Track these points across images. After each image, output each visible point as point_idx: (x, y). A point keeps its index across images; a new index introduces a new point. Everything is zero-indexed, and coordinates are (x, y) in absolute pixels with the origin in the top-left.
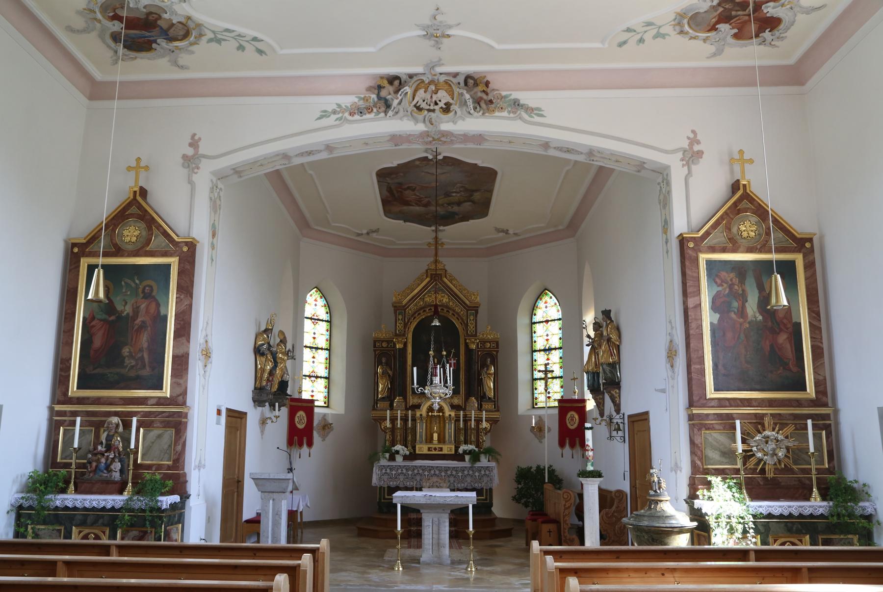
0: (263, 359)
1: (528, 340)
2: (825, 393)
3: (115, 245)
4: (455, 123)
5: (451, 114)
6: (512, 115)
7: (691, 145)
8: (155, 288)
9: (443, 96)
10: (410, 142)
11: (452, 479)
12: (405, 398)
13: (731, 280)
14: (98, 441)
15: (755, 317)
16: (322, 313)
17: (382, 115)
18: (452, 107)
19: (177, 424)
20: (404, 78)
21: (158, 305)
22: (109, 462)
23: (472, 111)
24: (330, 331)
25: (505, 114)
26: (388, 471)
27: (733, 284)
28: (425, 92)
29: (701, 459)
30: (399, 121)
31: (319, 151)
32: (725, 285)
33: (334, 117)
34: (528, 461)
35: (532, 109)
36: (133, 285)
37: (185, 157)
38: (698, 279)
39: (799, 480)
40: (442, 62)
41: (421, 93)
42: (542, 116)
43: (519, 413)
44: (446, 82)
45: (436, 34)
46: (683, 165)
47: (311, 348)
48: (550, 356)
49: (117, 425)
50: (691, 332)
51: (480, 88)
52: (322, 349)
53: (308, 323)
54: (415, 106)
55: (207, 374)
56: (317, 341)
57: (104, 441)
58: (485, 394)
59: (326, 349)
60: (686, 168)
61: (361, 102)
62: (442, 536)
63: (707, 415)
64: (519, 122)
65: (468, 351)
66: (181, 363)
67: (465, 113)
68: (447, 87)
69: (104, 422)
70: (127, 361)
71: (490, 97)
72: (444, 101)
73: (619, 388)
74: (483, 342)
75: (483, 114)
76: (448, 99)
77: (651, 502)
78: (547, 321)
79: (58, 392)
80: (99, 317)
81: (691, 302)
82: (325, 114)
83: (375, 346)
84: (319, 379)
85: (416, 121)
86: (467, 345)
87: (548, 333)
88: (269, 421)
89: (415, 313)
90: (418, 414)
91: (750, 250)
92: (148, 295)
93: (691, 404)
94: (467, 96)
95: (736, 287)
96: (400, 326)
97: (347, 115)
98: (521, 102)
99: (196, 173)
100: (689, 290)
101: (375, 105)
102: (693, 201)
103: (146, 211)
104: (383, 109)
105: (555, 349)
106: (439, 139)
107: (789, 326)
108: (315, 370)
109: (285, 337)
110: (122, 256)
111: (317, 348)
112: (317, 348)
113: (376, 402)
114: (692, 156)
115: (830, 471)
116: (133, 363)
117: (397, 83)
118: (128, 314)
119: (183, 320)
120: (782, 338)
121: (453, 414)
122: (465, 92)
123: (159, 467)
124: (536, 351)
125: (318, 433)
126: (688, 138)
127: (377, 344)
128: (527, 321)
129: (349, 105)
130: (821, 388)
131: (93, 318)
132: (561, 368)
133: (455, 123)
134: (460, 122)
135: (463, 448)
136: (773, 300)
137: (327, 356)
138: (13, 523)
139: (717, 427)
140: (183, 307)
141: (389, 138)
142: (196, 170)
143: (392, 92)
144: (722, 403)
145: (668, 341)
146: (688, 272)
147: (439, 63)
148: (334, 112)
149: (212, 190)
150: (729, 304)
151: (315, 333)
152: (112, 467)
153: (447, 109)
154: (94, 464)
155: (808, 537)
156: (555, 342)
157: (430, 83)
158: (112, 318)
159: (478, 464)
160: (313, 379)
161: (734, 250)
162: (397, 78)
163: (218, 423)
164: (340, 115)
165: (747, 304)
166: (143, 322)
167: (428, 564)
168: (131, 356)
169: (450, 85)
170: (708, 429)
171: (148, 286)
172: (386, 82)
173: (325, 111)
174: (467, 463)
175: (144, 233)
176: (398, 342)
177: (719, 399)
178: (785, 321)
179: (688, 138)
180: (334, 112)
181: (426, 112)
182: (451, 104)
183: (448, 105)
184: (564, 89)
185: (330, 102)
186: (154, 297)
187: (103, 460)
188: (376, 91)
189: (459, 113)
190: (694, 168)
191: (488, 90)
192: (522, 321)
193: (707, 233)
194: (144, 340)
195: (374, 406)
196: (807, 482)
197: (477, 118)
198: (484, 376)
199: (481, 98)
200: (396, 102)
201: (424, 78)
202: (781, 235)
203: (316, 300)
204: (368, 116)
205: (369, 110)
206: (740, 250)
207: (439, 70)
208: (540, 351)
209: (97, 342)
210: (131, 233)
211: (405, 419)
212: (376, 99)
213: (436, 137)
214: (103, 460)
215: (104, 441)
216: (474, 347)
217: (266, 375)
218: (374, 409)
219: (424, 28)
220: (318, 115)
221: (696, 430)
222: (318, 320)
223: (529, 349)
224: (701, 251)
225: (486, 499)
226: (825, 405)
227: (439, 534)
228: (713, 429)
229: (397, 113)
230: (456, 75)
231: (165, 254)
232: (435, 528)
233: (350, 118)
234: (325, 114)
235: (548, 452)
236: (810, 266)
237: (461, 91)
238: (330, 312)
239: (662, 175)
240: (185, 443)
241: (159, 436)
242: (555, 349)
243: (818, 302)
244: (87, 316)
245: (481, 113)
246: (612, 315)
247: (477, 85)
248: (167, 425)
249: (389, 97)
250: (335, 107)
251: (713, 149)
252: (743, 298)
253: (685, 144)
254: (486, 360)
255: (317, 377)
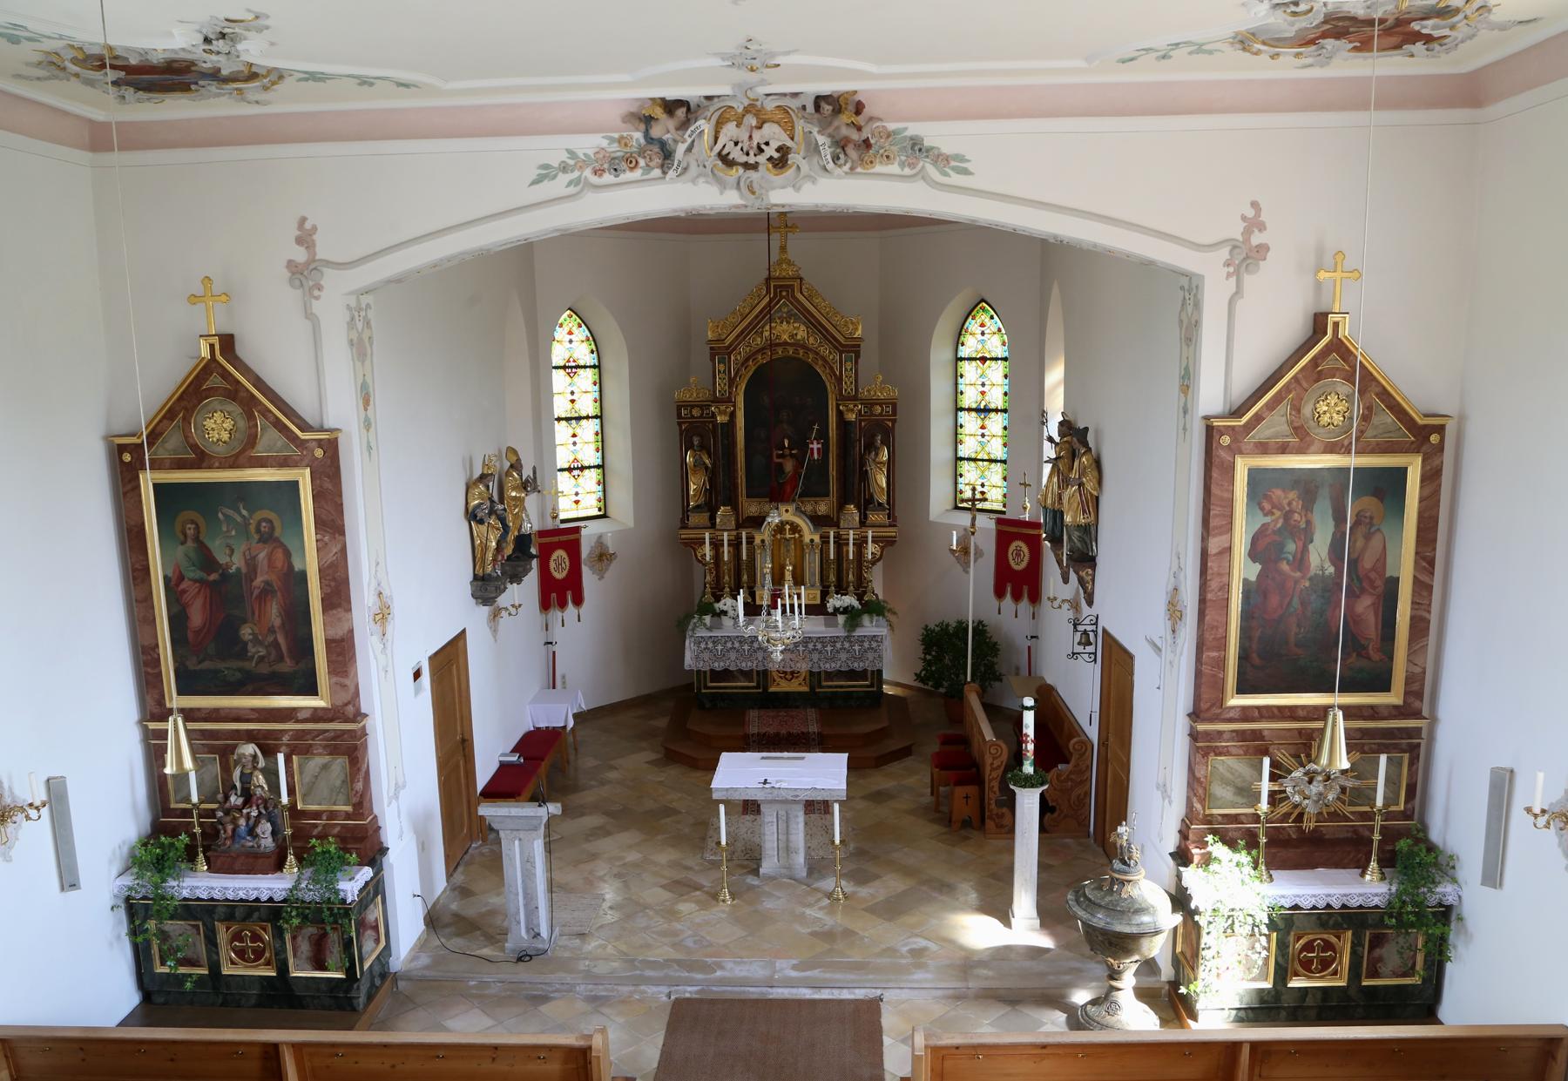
0: (484, 528)
1: (950, 389)
2: (1419, 695)
3: (195, 447)
4: (797, 188)
6: (907, 171)
7: (1247, 232)
8: (277, 523)
9: (774, 134)
11: (815, 656)
12: (735, 508)
13: (1289, 504)
14: (229, 787)
15: (1322, 569)
16: (584, 354)
17: (657, 172)
19: (349, 746)
21: (288, 554)
22: (252, 822)
23: (831, 166)
24: (600, 383)
25: (894, 168)
26: (710, 645)
27: (1292, 512)
29: (1202, 801)
32: (1278, 513)
33: (564, 178)
34: (941, 613)
35: (947, 159)
36: (239, 519)
37: (291, 265)
38: (1230, 503)
39: (1355, 830)
41: (730, 130)
42: (966, 172)
43: (932, 518)
46: (1229, 275)
47: (568, 419)
48: (987, 422)
49: (255, 757)
50: (1209, 596)
51: (845, 118)
52: (587, 417)
53: (559, 378)
55: (389, 645)
56: (577, 406)
57: (238, 784)
58: (871, 496)
59: (596, 417)
60: (1233, 280)
61: (615, 147)
62: (792, 838)
63: (1220, 733)
64: (920, 185)
65: (843, 424)
66: (343, 650)
67: (817, 168)
69: (235, 747)
70: (252, 649)
71: (866, 134)
72: (774, 145)
73: (1094, 567)
74: (870, 404)
75: (852, 169)
77: (1113, 881)
78: (983, 360)
79: (150, 702)
80: (191, 575)
81: (1215, 545)
82: (546, 173)
83: (679, 415)
84: (586, 472)
85: (723, 186)
86: (840, 414)
87: (986, 383)
88: (504, 613)
89: (747, 360)
90: (757, 541)
91: (1331, 449)
92: (268, 538)
93: (1195, 715)
95: (1297, 517)
96: (721, 385)
97: (588, 173)
98: (927, 143)
99: (317, 298)
100: (1213, 523)
101: (642, 152)
102: (1237, 347)
103: (238, 382)
104: (657, 161)
105: (997, 411)
107: (1379, 583)
108: (579, 457)
109: (519, 460)
110: (210, 467)
111: (579, 419)
112: (579, 419)
113: (686, 511)
114: (1247, 256)
115: (1406, 815)
116: (263, 652)
117: (681, 112)
118: (238, 569)
119: (334, 579)
120: (1365, 604)
121: (817, 538)
122: (815, 130)
123: (332, 815)
124: (962, 409)
125: (591, 568)
126: (1244, 218)
127: (683, 412)
128: (948, 355)
129: (591, 152)
130: (1415, 687)
131: (181, 578)
132: (1005, 445)
133: (797, 188)
134: (807, 187)
135: (835, 602)
136: (1324, 760)
137: (598, 428)
138: (124, 929)
139: (1234, 751)
140: (330, 558)
142: (316, 293)
144: (1246, 714)
145: (1171, 587)
146: (1215, 490)
148: (564, 168)
149: (351, 324)
150: (1281, 547)
151: (573, 392)
152: (259, 830)
153: (781, 161)
154: (230, 827)
155: (1349, 933)
156: (996, 398)
157: (747, 110)
158: (214, 577)
159: (859, 632)
160: (576, 473)
161: (1301, 450)
162: (680, 103)
163: (417, 691)
164: (576, 174)
165: (1311, 547)
166: (267, 583)
167: (771, 878)
168: (256, 641)
170: (1220, 754)
171: (264, 520)
173: (546, 167)
174: (839, 631)
175: (242, 424)
176: (721, 413)
177: (1244, 709)
178: (1373, 575)
179: (1244, 218)
180: (564, 168)
181: (741, 170)
183: (783, 150)
184: (1009, 115)
185: (554, 149)
186: (277, 540)
187: (242, 822)
190: (1248, 279)
192: (939, 356)
193: (1258, 418)
194: (274, 613)
195: (682, 520)
196: (1367, 833)
197: (839, 177)
198: (871, 468)
202: (1389, 418)
203: (570, 333)
206: (1313, 448)
208: (969, 410)
209: (196, 618)
210: (218, 426)
211: (736, 544)
212: (642, 141)
214: (242, 822)
215: (238, 784)
216: (852, 417)
217: (490, 556)
218: (684, 526)
220: (534, 173)
221: (1199, 757)
222: (578, 367)
223: (951, 406)
224: (1241, 453)
225: (872, 686)
226: (1417, 715)
227: (787, 833)
228: (1228, 753)
229: (685, 169)
231: (284, 463)
232: (782, 826)
233: (595, 180)
234: (546, 173)
235: (973, 595)
236: (1431, 477)
237: (809, 127)
238: (597, 350)
239: (1188, 288)
240: (367, 773)
241: (325, 767)
242: (997, 411)
243: (1435, 540)
244: (170, 575)
245: (846, 168)
246: (1090, 438)
248: (334, 751)
250: (564, 156)
251: (1284, 240)
252: (1307, 535)
253: (1236, 231)
254: (874, 436)
255: (582, 468)
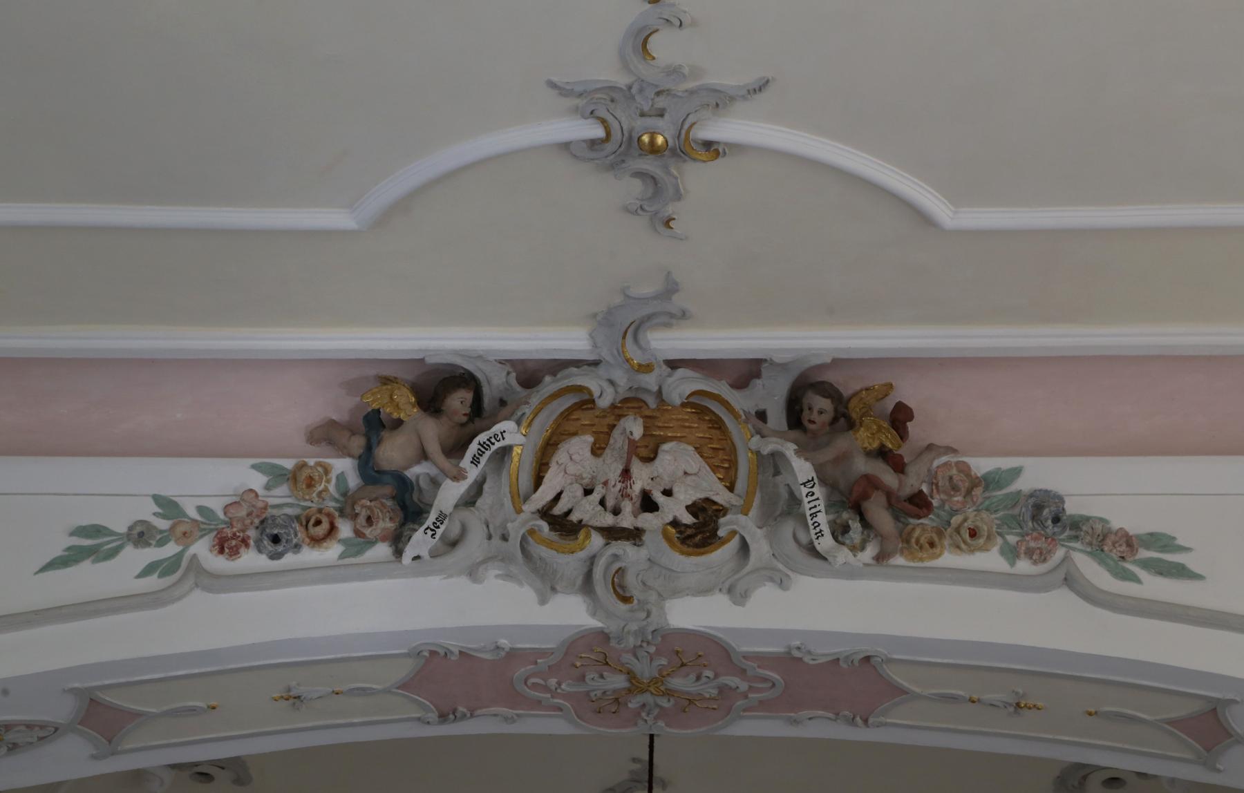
5: (723, 554)
6: (1024, 566)
9: (683, 473)
10: (514, 698)
17: (382, 550)
18: (725, 526)
20: (495, 381)
23: (826, 543)
25: (990, 560)
28: (597, 451)
30: (463, 581)
31: (46, 732)
33: (135, 557)
35: (1130, 542)
40: (678, 301)
41: (575, 455)
42: (1180, 572)
44: (697, 406)
45: (646, 140)
51: (864, 438)
54: (545, 513)
61: (281, 495)
64: (1063, 598)
68: (701, 431)
71: (915, 481)
72: (686, 495)
75: (880, 558)
76: (711, 487)
82: (92, 544)
85: (548, 583)
94: (802, 469)
97: (202, 549)
98: (1072, 508)
101: (348, 506)
104: (386, 524)
106: (658, 684)
117: (459, 402)
122: (789, 449)
129: (217, 506)
133: (738, 595)
141: (404, 670)
143: (434, 448)
147: (667, 307)
148: (141, 535)
153: (701, 529)
157: (617, 411)
164: (171, 549)
169: (718, 424)
172: (405, 398)
180: (141, 535)
181: (597, 540)
182: (722, 511)
185: (120, 489)
188: (358, 443)
189: (760, 547)
191: (905, 451)
197: (850, 573)
199: (871, 483)
200: (450, 494)
201: (592, 382)
204: (310, 556)
205: (318, 528)
207: (666, 342)
212: (353, 481)
213: (645, 670)
219: (589, 99)
220: (59, 544)
230: (747, 372)
233: (219, 563)
234: (92, 544)
247: (851, 425)
249: (418, 471)
250: (147, 511)
